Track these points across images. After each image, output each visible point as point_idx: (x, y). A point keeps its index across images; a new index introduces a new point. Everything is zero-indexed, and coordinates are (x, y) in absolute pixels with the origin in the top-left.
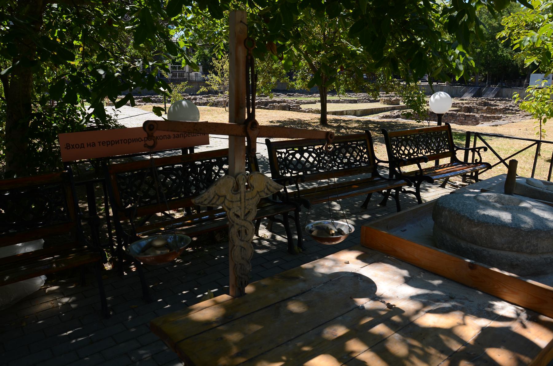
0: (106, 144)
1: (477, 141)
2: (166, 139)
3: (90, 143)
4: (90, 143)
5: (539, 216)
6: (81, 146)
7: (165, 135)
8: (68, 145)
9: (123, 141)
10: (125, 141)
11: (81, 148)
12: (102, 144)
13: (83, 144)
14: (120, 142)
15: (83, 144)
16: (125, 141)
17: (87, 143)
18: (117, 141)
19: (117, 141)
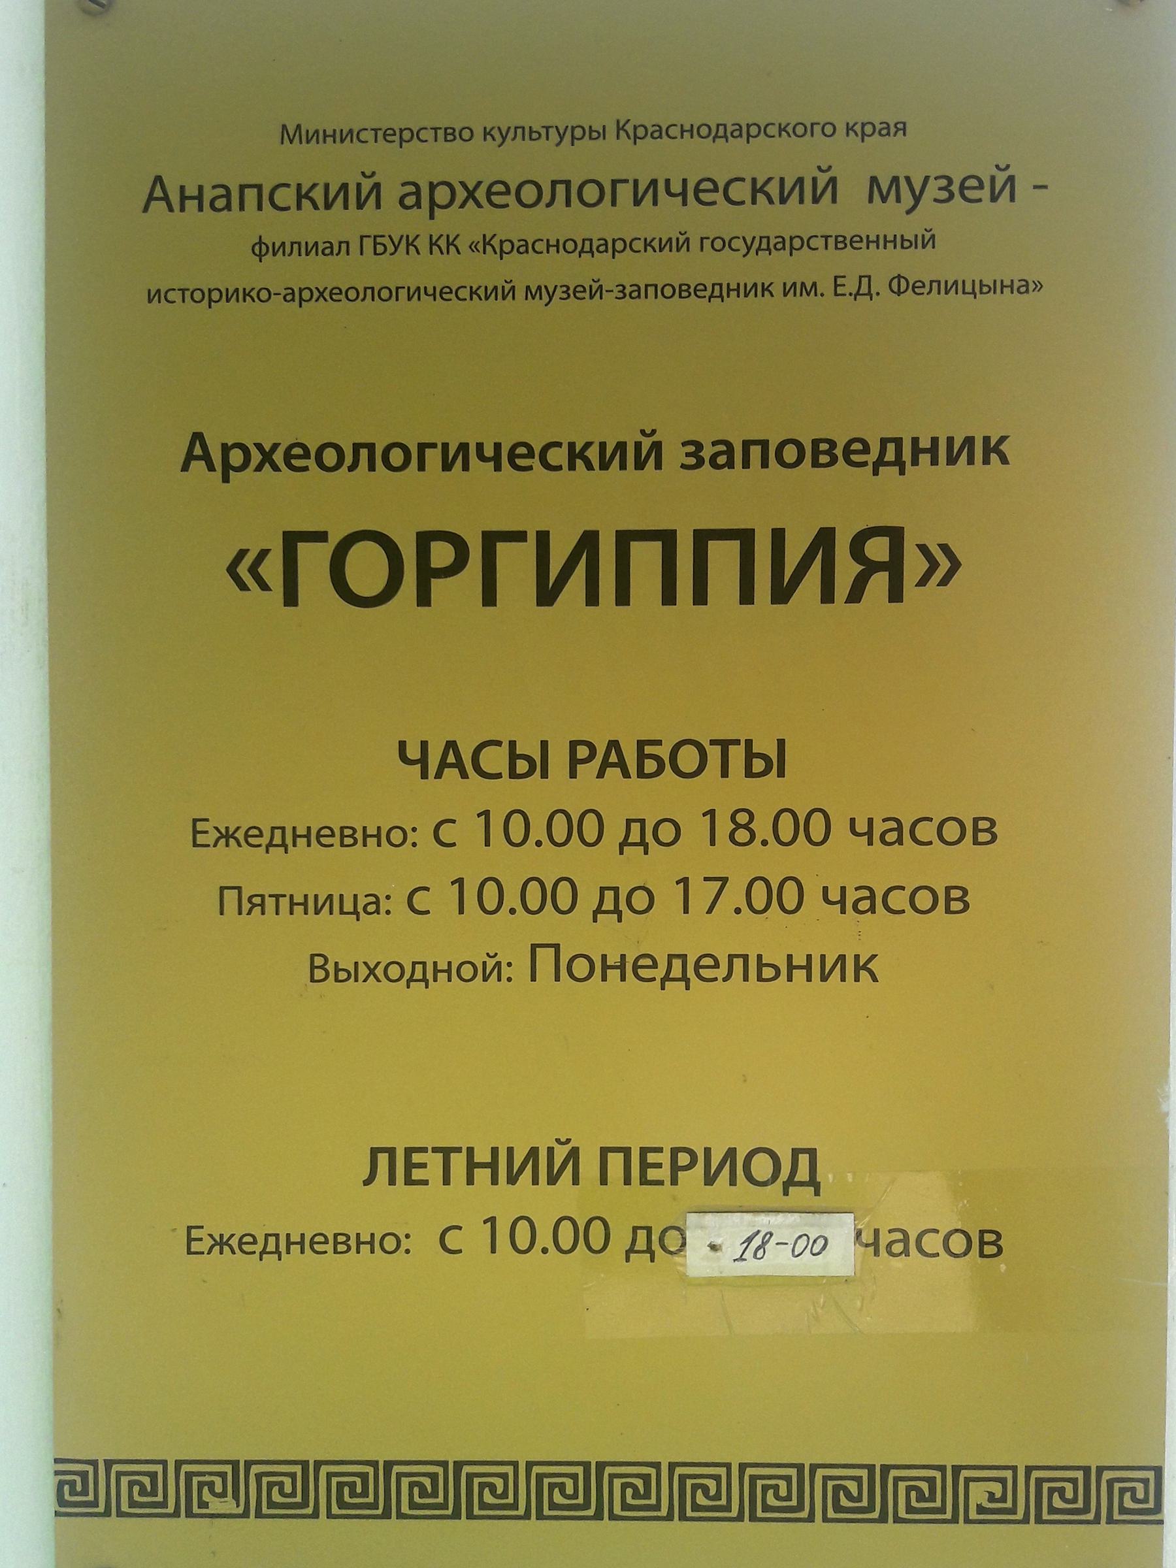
0: (397, 138)
1: (468, 204)
2: (765, 464)
3: (201, 188)
4: (201, 188)
5: (46, 210)
6: (718, 130)
7: (587, 237)
8: (319, 961)
9: (188, 294)
10: (198, 295)
11: (714, 138)
12: (385, 135)
13: (812, 1153)
14: (270, 903)
15: (812, 1153)
16: (198, 295)
17: (263, 913)
18: (277, 245)
19: (277, 245)
